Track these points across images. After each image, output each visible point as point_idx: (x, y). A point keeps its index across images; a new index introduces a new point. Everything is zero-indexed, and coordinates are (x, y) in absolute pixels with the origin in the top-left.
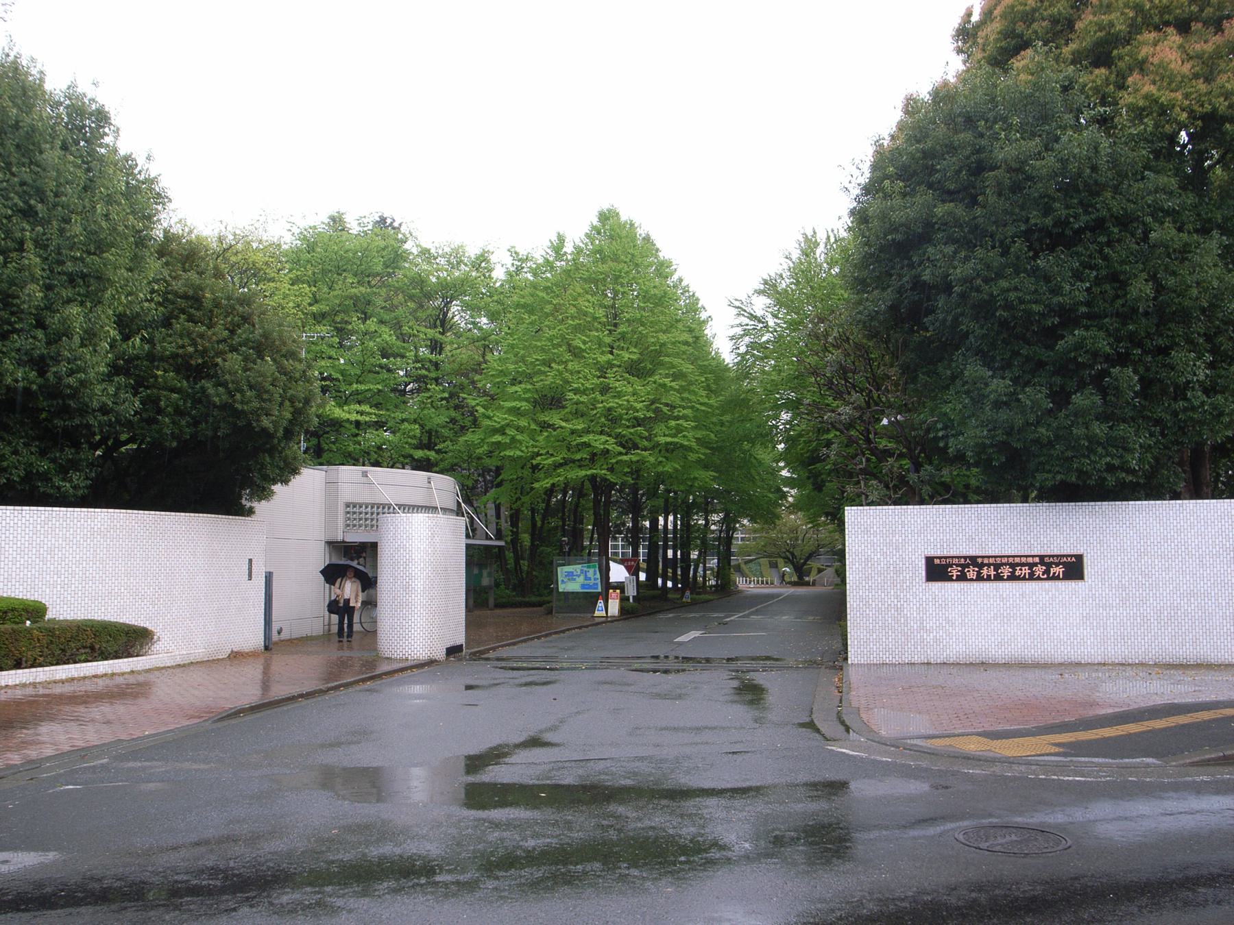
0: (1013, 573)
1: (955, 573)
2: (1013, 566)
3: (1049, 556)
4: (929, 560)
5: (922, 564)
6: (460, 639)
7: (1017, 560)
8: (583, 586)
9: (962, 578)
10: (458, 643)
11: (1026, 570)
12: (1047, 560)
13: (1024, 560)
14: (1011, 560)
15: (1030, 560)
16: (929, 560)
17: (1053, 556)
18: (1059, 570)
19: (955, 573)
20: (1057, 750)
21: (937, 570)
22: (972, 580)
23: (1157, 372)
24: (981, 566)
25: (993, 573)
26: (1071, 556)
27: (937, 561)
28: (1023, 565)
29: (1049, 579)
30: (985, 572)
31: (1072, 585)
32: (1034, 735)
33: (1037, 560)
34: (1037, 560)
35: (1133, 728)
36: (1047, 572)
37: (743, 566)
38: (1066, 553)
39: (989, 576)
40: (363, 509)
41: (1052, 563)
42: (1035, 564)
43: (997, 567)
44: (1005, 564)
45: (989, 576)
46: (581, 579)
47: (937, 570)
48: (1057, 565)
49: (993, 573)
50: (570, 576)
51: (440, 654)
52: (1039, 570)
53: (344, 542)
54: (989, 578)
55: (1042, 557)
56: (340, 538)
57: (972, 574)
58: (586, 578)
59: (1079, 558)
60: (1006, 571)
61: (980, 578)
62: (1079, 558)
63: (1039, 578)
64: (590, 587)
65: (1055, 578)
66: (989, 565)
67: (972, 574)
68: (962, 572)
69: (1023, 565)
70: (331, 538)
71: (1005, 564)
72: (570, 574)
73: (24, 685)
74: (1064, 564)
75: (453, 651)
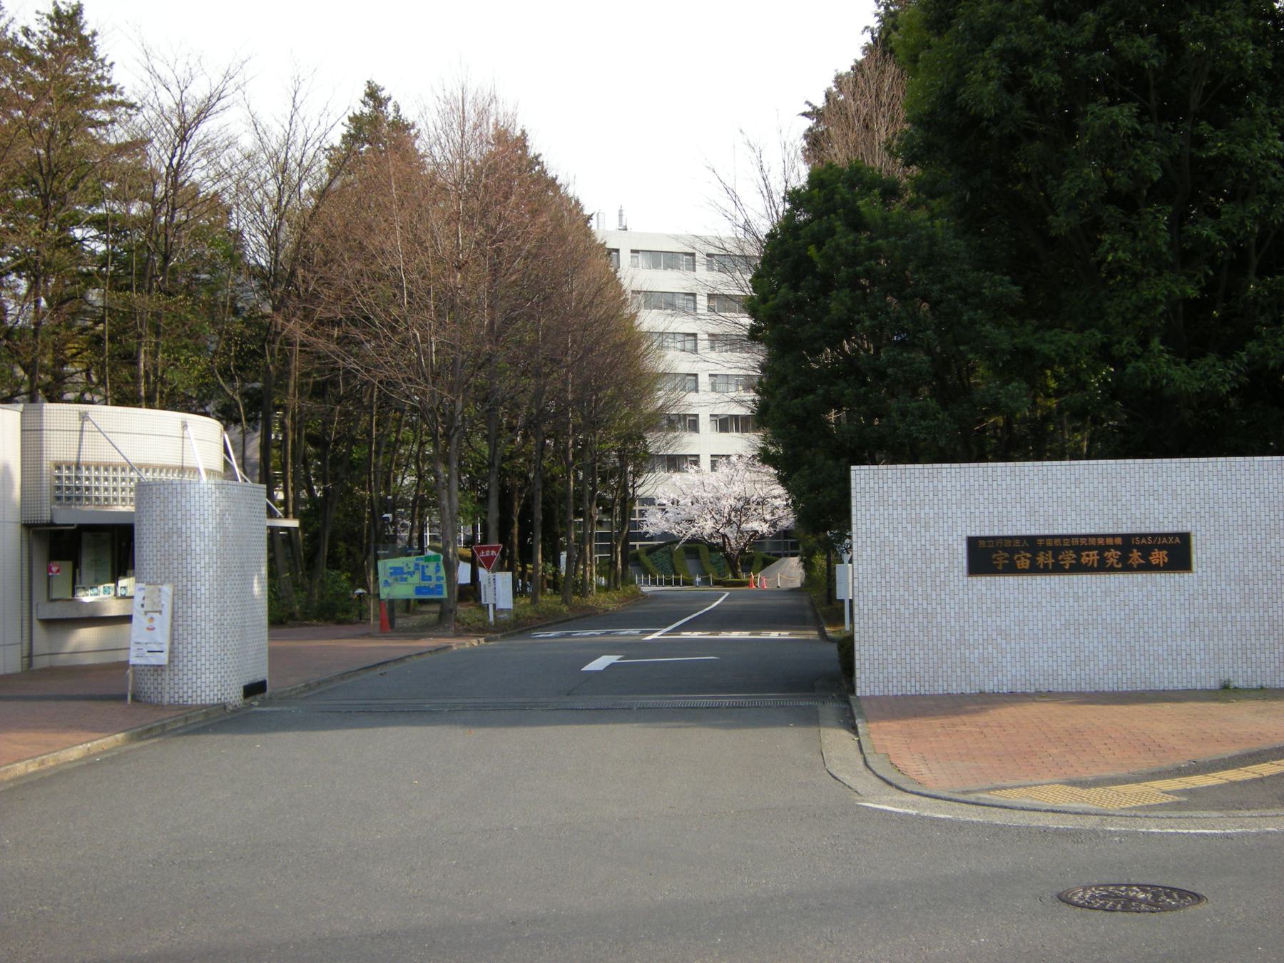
2: (1078, 550)
4: (973, 542)
5: (962, 549)
6: (261, 673)
8: (419, 590)
10: (260, 678)
14: (1101, 541)
16: (973, 542)
18: (1159, 557)
20: (1171, 799)
21: (989, 556)
23: (347, 277)
25: (1051, 561)
26: (1114, 536)
31: (1175, 578)
32: (1137, 781)
35: (1266, 769)
36: (1033, 561)
37: (643, 557)
38: (1166, 530)
39: (1046, 565)
42: (1107, 548)
44: (1068, 548)
45: (1046, 565)
46: (416, 579)
47: (989, 556)
49: (1051, 561)
50: (398, 573)
51: (234, 695)
52: (1112, 556)
53: (52, 524)
56: (46, 518)
57: (1024, 563)
58: (425, 577)
59: (1185, 538)
62: (1185, 538)
63: (1112, 570)
64: (430, 591)
67: (1024, 563)
69: (1090, 548)
70: (33, 518)
72: (397, 572)
73: (104, 752)
75: (254, 689)
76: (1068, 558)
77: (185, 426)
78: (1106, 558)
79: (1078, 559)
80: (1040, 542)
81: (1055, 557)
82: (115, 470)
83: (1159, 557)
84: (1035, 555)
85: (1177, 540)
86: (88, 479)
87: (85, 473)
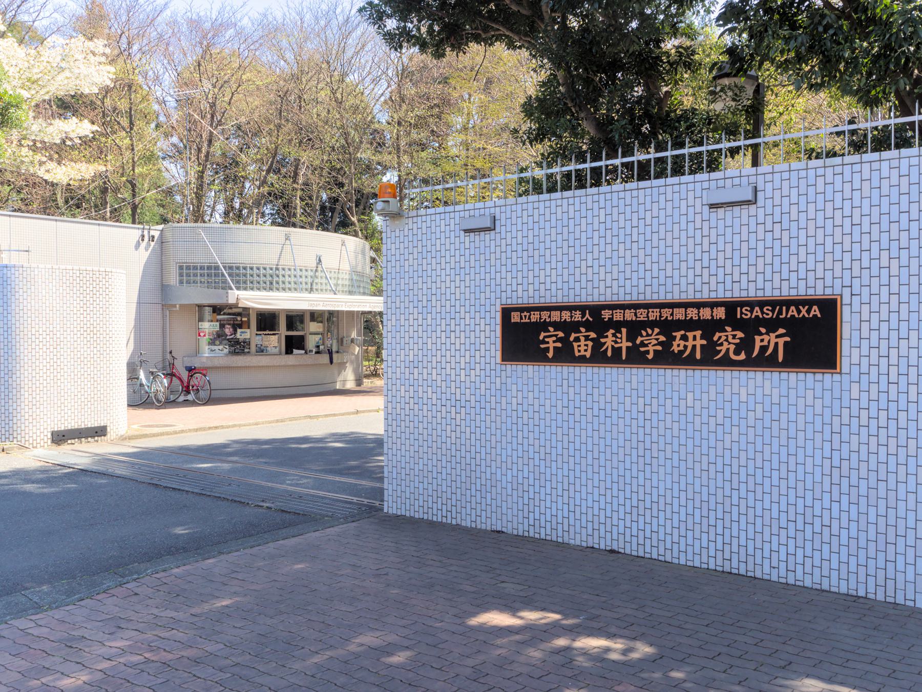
0: (667, 345)
1: (552, 344)
2: (668, 327)
3: (612, 307)
7: (679, 314)
9: (565, 355)
11: (695, 340)
12: (745, 314)
13: (692, 313)
15: (706, 313)
17: (762, 304)
18: (774, 341)
19: (552, 344)
22: (582, 360)
24: (750, 328)
25: (625, 344)
27: (515, 317)
28: (689, 325)
29: (751, 363)
30: (609, 341)
33: (720, 313)
34: (720, 313)
36: (745, 345)
39: (617, 351)
40: (304, 273)
41: (759, 322)
43: (634, 328)
45: (617, 351)
48: (771, 325)
49: (625, 344)
52: (728, 339)
54: (616, 358)
55: (731, 306)
57: (583, 348)
60: (652, 341)
61: (599, 357)
62: (829, 307)
63: (727, 362)
65: (766, 361)
66: (617, 326)
67: (583, 348)
68: (565, 341)
69: (689, 325)
71: (652, 324)
74: (792, 325)
76: (652, 341)
77: (343, 244)
78: (716, 344)
79: (667, 345)
80: (606, 315)
81: (631, 337)
82: (301, 270)
83: (774, 341)
84: (601, 334)
85: (816, 311)
86: (252, 276)
87: (281, 272)
